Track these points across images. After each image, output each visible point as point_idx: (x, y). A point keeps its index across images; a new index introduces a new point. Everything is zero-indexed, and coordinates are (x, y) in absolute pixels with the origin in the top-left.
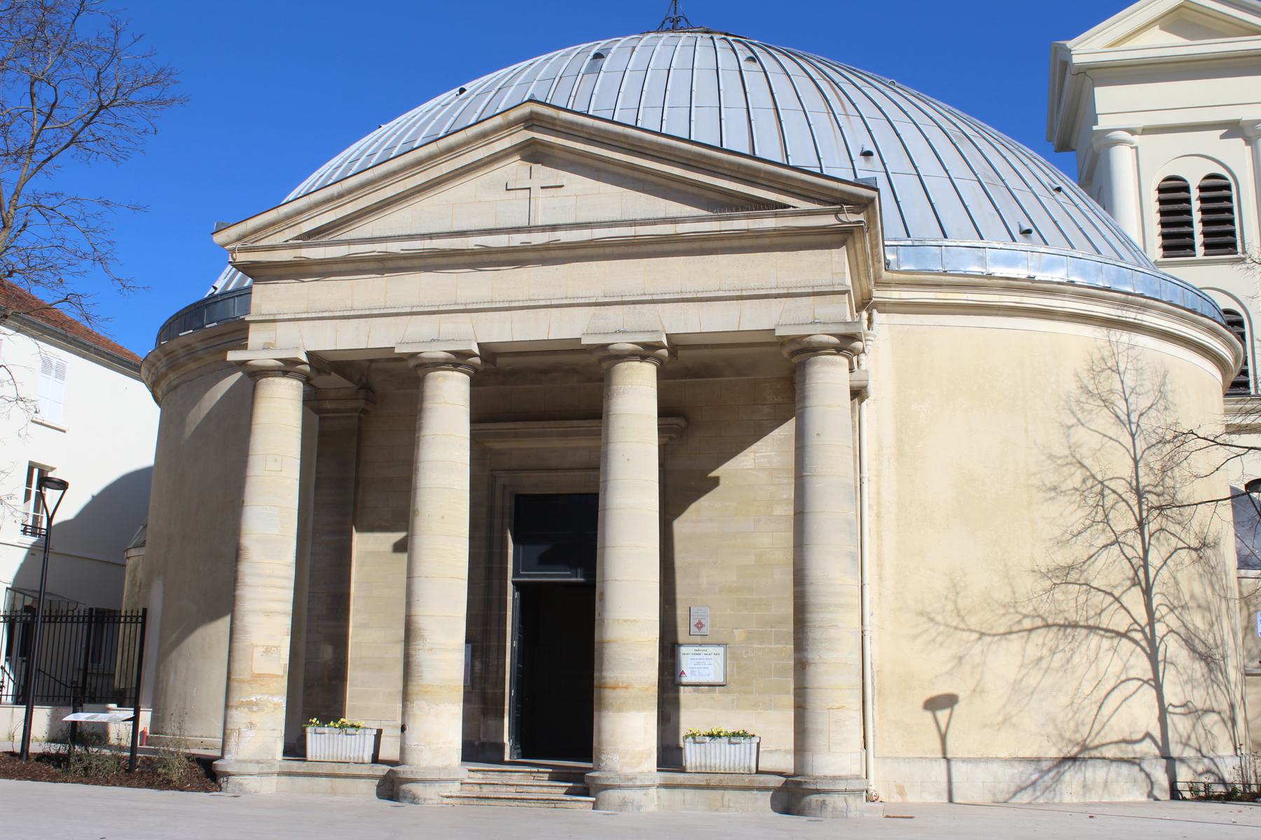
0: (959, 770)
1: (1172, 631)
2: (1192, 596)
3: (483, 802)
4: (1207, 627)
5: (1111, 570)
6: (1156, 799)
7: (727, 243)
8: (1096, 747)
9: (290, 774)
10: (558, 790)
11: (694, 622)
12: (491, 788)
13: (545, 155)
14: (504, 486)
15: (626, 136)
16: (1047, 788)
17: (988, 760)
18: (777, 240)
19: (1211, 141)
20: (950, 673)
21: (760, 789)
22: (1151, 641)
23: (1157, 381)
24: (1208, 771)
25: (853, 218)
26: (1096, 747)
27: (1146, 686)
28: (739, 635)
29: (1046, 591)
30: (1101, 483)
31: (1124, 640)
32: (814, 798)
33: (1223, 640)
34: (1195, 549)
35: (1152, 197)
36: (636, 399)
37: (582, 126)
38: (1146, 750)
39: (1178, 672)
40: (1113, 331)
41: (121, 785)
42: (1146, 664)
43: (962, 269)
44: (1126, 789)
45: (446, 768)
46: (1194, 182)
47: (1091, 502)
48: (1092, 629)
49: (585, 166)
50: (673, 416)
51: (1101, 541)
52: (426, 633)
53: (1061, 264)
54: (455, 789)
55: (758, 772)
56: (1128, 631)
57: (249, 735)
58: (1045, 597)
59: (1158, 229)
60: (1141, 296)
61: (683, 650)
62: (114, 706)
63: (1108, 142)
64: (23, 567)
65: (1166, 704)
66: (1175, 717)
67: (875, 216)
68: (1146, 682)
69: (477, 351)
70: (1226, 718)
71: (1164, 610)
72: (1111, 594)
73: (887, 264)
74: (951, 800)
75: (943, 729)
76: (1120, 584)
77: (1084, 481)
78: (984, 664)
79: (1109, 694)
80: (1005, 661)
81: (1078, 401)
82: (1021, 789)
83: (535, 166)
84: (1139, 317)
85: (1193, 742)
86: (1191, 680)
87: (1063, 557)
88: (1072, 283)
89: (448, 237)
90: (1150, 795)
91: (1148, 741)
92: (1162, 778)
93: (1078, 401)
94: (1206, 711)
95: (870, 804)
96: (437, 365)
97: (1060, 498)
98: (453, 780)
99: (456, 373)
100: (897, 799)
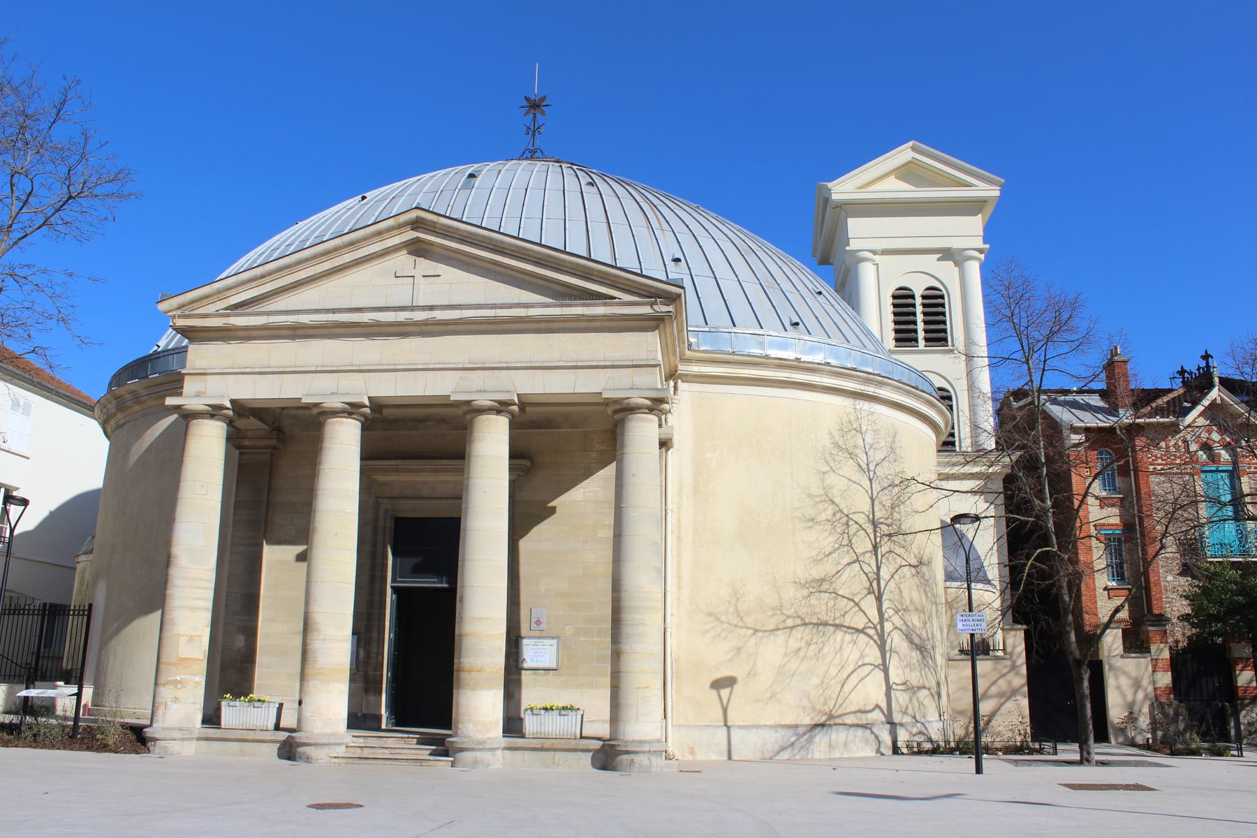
0: (736, 734)
2: (912, 602)
5: (853, 581)
8: (839, 716)
9: (206, 739)
10: (425, 752)
11: (533, 620)
13: (427, 251)
14: (386, 511)
15: (491, 239)
19: (930, 263)
20: (731, 660)
21: (583, 751)
22: (881, 635)
23: (889, 439)
24: (920, 733)
25: (665, 309)
26: (839, 716)
28: (569, 630)
32: (625, 757)
36: (492, 445)
42: (878, 654)
43: (746, 351)
45: (334, 734)
47: (839, 530)
53: (820, 350)
54: (341, 751)
55: (581, 737)
59: (892, 326)
61: (525, 642)
62: (61, 683)
71: (891, 612)
72: (852, 600)
73: (690, 345)
74: (730, 758)
80: (773, 651)
81: (831, 454)
82: (783, 749)
85: (910, 711)
86: (909, 665)
87: (817, 572)
88: (828, 364)
90: (878, 751)
92: (886, 738)
93: (831, 454)
94: (920, 688)
96: (335, 413)
98: (340, 744)
100: (689, 757)
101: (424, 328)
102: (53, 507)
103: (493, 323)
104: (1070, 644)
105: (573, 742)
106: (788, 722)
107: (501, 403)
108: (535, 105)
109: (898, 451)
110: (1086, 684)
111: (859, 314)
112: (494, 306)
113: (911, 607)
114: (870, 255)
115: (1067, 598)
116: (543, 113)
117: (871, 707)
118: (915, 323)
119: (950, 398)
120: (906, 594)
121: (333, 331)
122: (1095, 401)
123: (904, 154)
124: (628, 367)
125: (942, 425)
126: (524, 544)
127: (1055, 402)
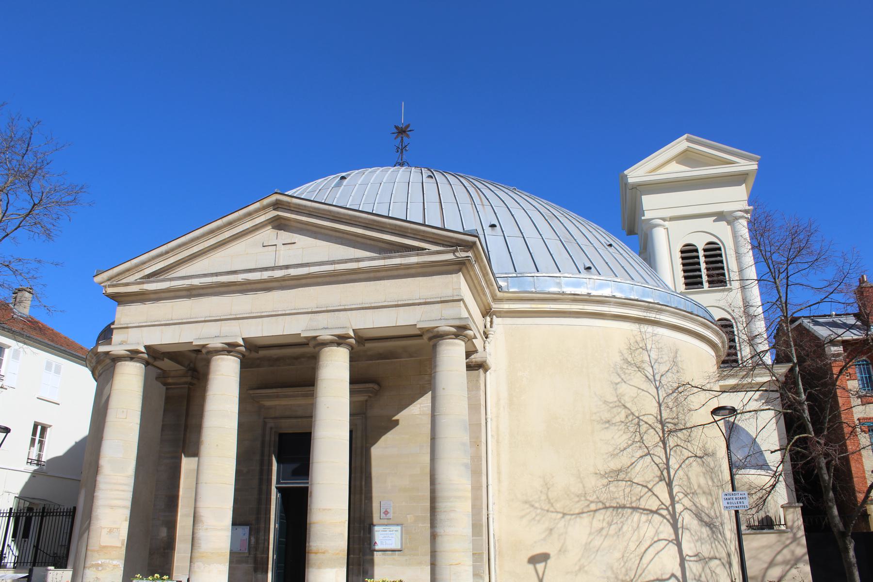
1: (686, 508)
2: (699, 486)
4: (710, 506)
5: (646, 471)
13: (286, 225)
14: (271, 428)
18: (420, 270)
19: (708, 224)
20: (544, 539)
22: (673, 515)
23: (672, 355)
25: (464, 254)
27: (671, 544)
28: (410, 518)
30: (638, 417)
31: (656, 516)
33: (720, 513)
34: (700, 457)
36: (335, 372)
37: (305, 206)
40: (642, 326)
42: (671, 531)
46: (700, 247)
47: (632, 430)
49: (308, 230)
51: (640, 453)
52: (203, 519)
53: (607, 286)
56: (658, 509)
58: (604, 490)
59: (682, 274)
61: (376, 528)
62: (52, 568)
63: (651, 226)
64: (27, 484)
66: (690, 563)
67: (480, 255)
70: (725, 562)
71: (681, 495)
72: (646, 487)
73: (500, 287)
77: (627, 417)
78: (566, 533)
79: (647, 549)
80: (579, 531)
81: (622, 368)
84: (658, 316)
86: (700, 539)
87: (615, 464)
88: (614, 297)
89: (246, 282)
91: (673, 579)
93: (622, 368)
94: (711, 559)
96: (218, 352)
97: (612, 428)
101: (283, 283)
103: (334, 276)
104: (833, 517)
107: (339, 337)
108: (402, 131)
110: (852, 553)
111: (655, 270)
112: (333, 262)
114: (661, 222)
115: (826, 477)
116: (408, 136)
117: (668, 576)
118: (700, 270)
119: (731, 326)
120: (694, 480)
121: (217, 290)
122: (851, 320)
123: (681, 144)
125: (720, 345)
126: (381, 451)
127: (817, 323)
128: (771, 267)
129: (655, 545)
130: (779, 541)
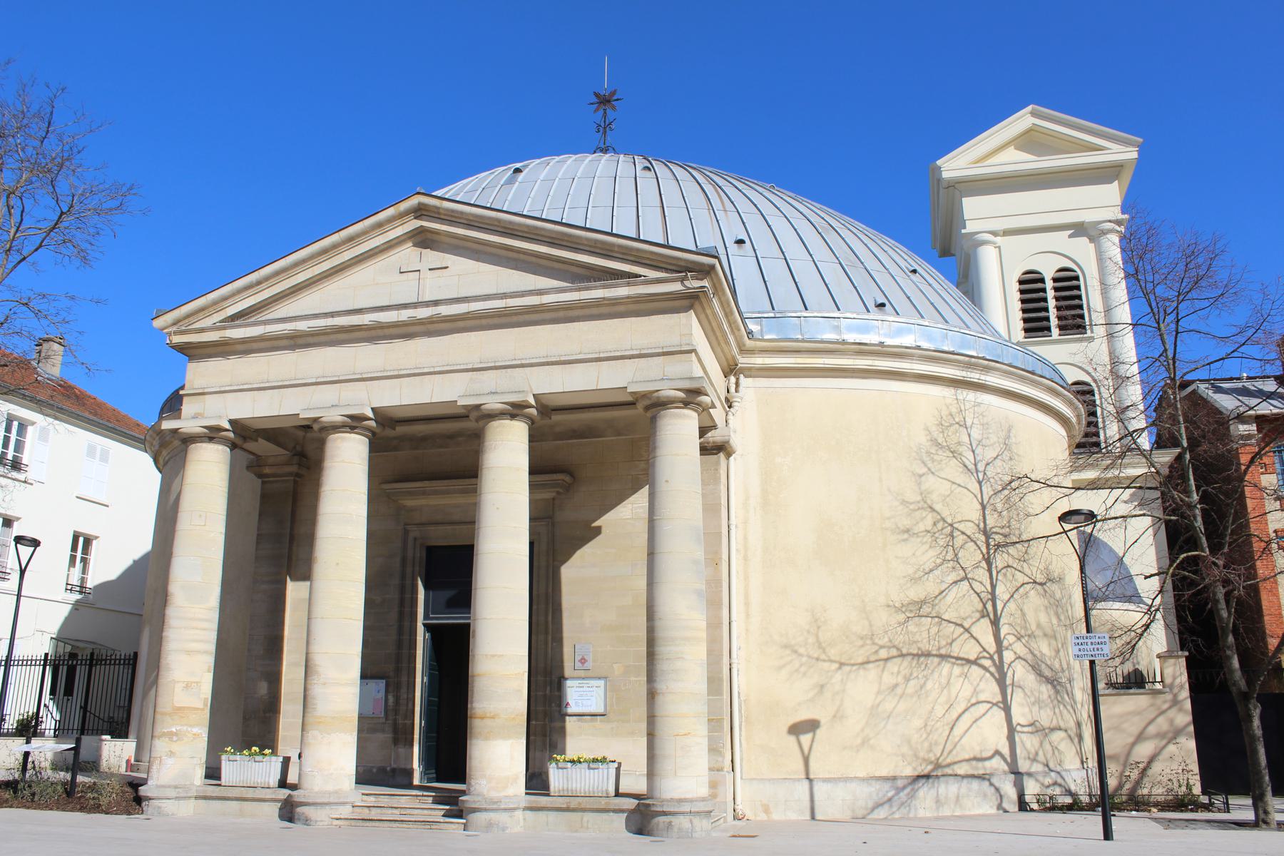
0: (820, 789)
2: (1039, 626)
3: (368, 824)
4: (1053, 654)
5: (961, 603)
6: (1006, 811)
7: (587, 312)
8: (948, 765)
9: (205, 798)
10: (438, 812)
11: (578, 658)
12: (379, 810)
13: (433, 241)
14: (415, 539)
15: (499, 220)
16: (903, 804)
17: (846, 779)
19: (1061, 240)
21: (615, 811)
22: (1000, 667)
23: (1002, 434)
24: (1055, 783)
26: (948, 765)
27: (995, 708)
28: (618, 669)
29: (900, 624)
31: (974, 667)
32: (661, 819)
33: (1068, 664)
34: (1041, 584)
35: (1014, 287)
36: (508, 458)
37: (462, 213)
38: (996, 766)
39: (1026, 694)
40: (959, 391)
41: (58, 809)
42: (996, 689)
43: (819, 337)
44: (977, 802)
45: (336, 792)
46: (1049, 275)
48: (942, 657)
50: (542, 468)
51: (953, 577)
53: (909, 331)
54: (346, 811)
55: (617, 794)
57: (169, 762)
60: (984, 359)
61: (569, 683)
62: (108, 737)
64: (67, 619)
65: (1014, 723)
68: (994, 704)
69: (371, 415)
71: (1011, 639)
72: (961, 625)
73: (750, 333)
74: (813, 818)
75: (806, 752)
76: (969, 616)
77: (935, 524)
78: (844, 691)
79: (960, 716)
80: (863, 689)
81: (928, 453)
82: (878, 805)
83: (424, 251)
84: (983, 377)
85: (1041, 757)
86: (1038, 702)
87: (915, 593)
88: (918, 348)
89: (376, 324)
90: (1000, 807)
92: (1010, 792)
93: (928, 453)
95: (737, 822)
96: (336, 428)
97: (913, 539)
98: (344, 803)
99: (353, 435)
100: (763, 817)
102: (137, 556)
103: (505, 315)
104: (1232, 671)
105: (603, 801)
106: (884, 773)
107: (513, 405)
108: (604, 101)
109: (1014, 448)
110: (1256, 722)
112: (504, 296)
113: (1038, 633)
115: (1224, 614)
116: (614, 108)
119: (1091, 393)
120: (1031, 617)
123: (1022, 120)
124: (658, 355)
125: (1074, 420)
127: (1219, 390)
128: (1154, 305)
129: (972, 709)
130: (1152, 705)
